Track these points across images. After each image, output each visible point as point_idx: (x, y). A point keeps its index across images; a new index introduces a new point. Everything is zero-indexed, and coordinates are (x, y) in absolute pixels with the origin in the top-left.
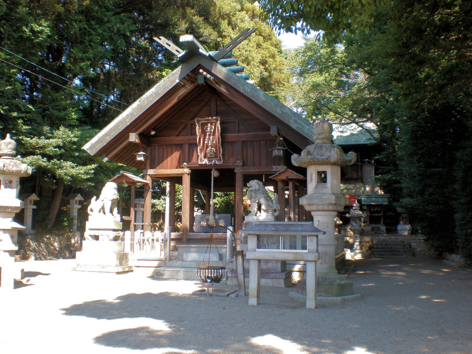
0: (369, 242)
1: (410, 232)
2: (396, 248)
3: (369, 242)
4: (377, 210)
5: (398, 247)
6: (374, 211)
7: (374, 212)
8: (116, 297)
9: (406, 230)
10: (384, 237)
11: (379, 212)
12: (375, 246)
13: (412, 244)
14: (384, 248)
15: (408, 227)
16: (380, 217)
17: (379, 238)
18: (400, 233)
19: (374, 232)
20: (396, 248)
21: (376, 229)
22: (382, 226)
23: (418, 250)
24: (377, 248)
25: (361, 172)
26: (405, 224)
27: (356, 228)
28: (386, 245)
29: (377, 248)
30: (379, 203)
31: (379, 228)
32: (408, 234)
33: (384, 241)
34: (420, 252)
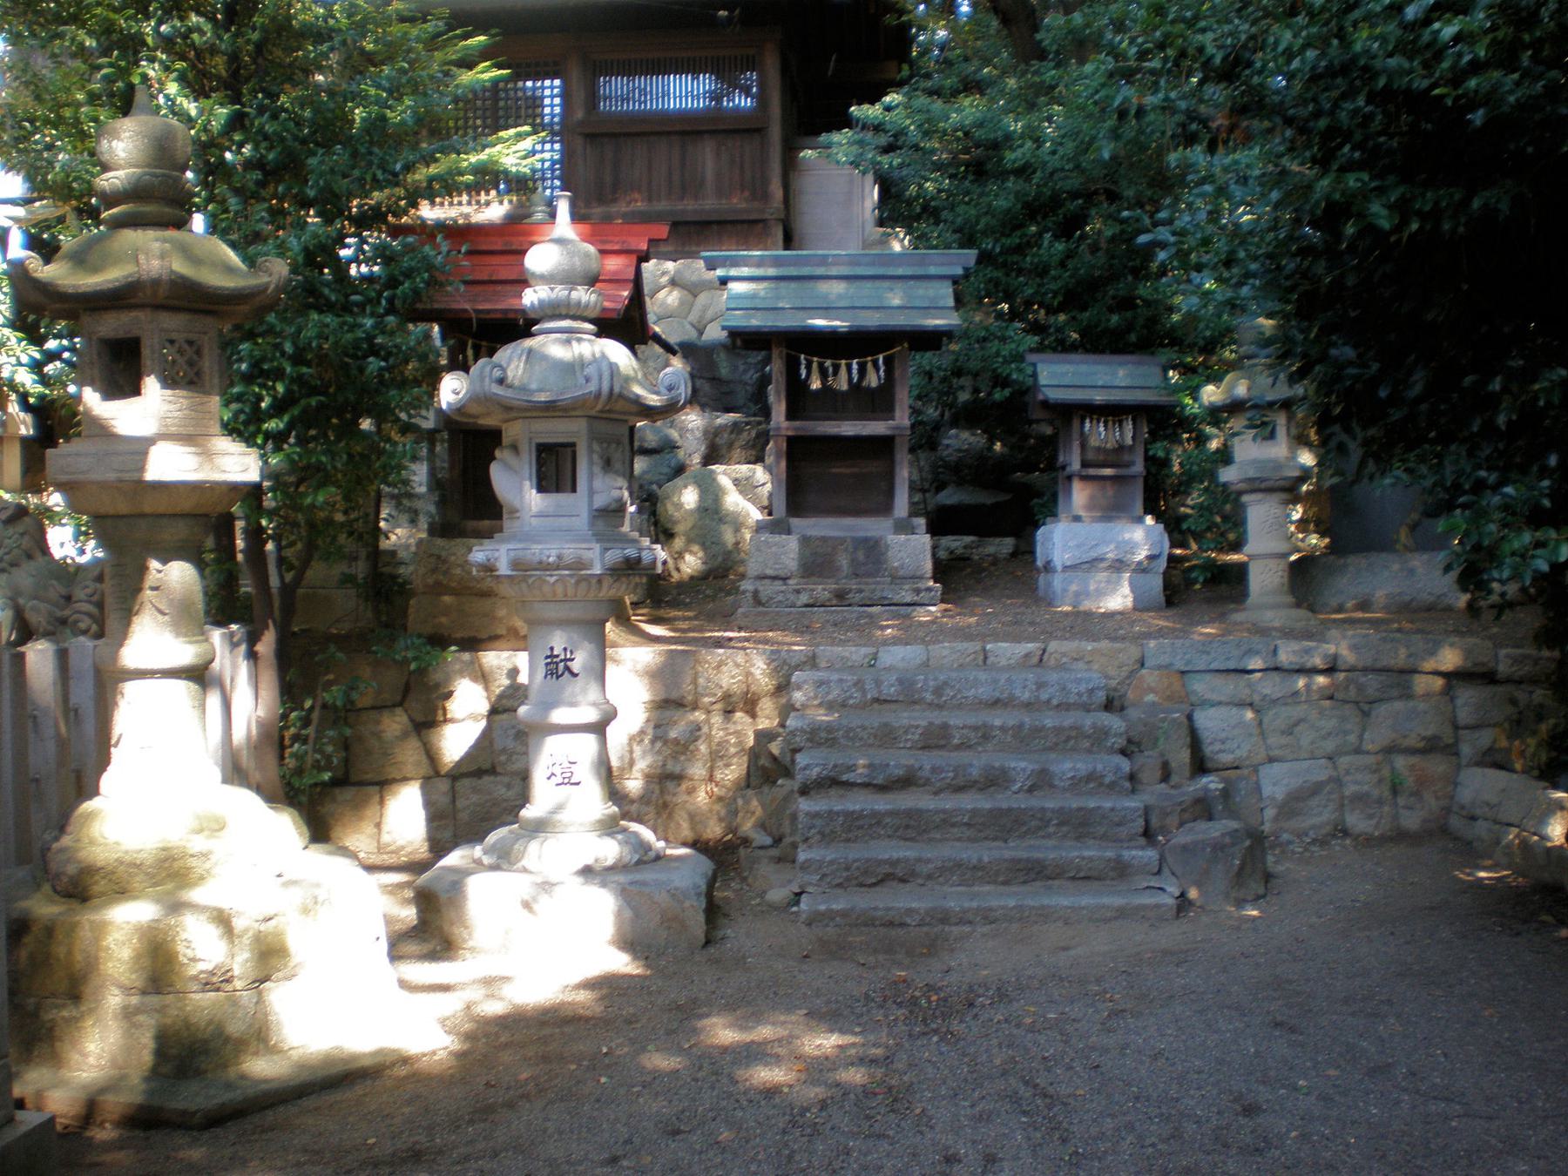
0: (750, 704)
1: (1156, 582)
2: (1041, 781)
3: (750, 704)
4: (856, 388)
5: (1067, 766)
6: (826, 389)
7: (831, 404)
8: (193, 715)
9: (1118, 566)
10: (925, 644)
11: (878, 402)
12: (810, 763)
13: (1209, 722)
14: (906, 782)
15: (1142, 537)
16: (882, 447)
17: (857, 653)
18: (1065, 592)
19: (822, 590)
20: (1041, 781)
21: (843, 561)
22: (903, 527)
23: (1276, 782)
24: (832, 782)
25: (786, 187)
26: (1112, 511)
27: (549, 551)
28: (936, 739)
29: (832, 782)
30: (872, 320)
31: (872, 551)
32: (1140, 606)
33: (909, 696)
34: (1293, 804)
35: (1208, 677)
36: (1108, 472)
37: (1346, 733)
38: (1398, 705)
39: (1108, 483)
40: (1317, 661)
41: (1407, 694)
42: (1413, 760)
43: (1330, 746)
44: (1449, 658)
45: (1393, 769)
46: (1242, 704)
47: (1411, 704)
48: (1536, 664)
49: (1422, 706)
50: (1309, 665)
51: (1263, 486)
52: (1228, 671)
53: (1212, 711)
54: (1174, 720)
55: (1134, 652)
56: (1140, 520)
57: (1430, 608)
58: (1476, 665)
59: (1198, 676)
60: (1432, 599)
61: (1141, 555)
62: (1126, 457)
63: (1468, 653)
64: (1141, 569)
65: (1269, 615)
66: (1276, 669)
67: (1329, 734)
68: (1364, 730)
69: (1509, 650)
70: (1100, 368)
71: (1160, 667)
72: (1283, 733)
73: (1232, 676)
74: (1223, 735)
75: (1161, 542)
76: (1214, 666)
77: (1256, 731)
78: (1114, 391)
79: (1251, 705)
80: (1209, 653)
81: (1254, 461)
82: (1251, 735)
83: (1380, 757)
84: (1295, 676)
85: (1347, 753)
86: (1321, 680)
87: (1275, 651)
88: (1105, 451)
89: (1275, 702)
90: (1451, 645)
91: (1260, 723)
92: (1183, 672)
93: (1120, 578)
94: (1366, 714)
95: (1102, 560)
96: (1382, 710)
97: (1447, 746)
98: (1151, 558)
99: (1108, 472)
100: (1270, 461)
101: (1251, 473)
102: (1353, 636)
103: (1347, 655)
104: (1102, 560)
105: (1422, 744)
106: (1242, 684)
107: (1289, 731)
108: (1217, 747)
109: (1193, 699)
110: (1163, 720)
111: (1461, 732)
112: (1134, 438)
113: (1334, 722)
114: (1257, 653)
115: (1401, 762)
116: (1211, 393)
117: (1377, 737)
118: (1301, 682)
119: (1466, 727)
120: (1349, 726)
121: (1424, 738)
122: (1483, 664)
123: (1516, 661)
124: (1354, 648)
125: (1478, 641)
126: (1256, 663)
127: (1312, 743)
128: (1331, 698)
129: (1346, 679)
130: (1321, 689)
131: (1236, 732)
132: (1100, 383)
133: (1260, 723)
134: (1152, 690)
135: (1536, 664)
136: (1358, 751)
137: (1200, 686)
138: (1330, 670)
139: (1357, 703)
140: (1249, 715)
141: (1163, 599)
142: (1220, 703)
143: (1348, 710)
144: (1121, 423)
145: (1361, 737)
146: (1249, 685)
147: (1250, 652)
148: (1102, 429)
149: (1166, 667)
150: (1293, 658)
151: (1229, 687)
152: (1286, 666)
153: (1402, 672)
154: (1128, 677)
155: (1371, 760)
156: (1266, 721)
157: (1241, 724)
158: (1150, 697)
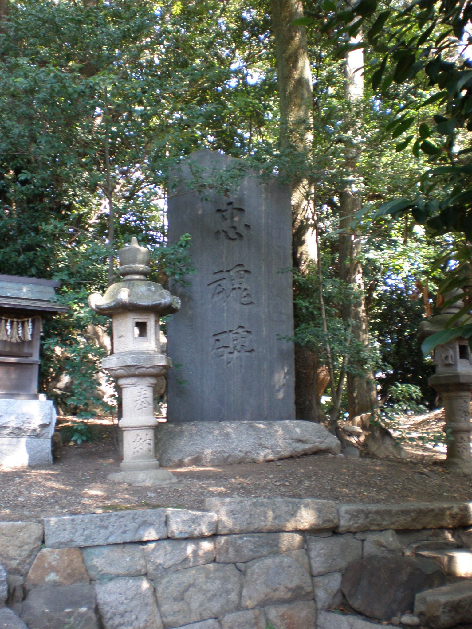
1: (47, 445)
9: (18, 432)
35: (106, 551)
36: (12, 360)
37: (228, 592)
38: (268, 562)
39: (12, 368)
40: (205, 529)
41: (275, 551)
42: (283, 609)
43: (216, 606)
44: (307, 518)
45: (267, 620)
46: (137, 575)
47: (277, 560)
48: (367, 517)
49: (286, 561)
50: (196, 533)
51: (137, 372)
52: (125, 543)
53: (111, 585)
54: (82, 615)
55: (35, 529)
56: (36, 397)
57: (240, 462)
58: (325, 521)
59: (97, 551)
60: (242, 455)
61: (35, 424)
62: (26, 350)
63: (319, 511)
64: (35, 435)
65: (141, 476)
66: (168, 538)
67: (214, 595)
68: (242, 587)
69: (352, 507)
70: (10, 285)
71: (60, 545)
72: (175, 599)
73: (128, 548)
74: (122, 608)
75: (51, 414)
76: (112, 540)
77: (151, 600)
78: (19, 300)
79: (146, 575)
80: (106, 528)
81: (131, 352)
82: (147, 604)
83: (257, 612)
84: (183, 544)
85: (230, 611)
86: (206, 546)
87: (166, 523)
88: (11, 343)
89: (166, 570)
90: (306, 506)
91: (155, 590)
92: (82, 548)
93: (18, 442)
94: (243, 573)
95: (5, 427)
96: (256, 567)
97: (308, 593)
98: (44, 426)
99: (12, 360)
100: (142, 353)
101: (129, 362)
102: (230, 503)
103: (228, 522)
104: (5, 427)
105: (288, 595)
106: (138, 555)
107: (181, 598)
108: (117, 620)
109: (93, 573)
110: (70, 615)
111: (317, 579)
112: (32, 335)
113: (217, 583)
114: (151, 524)
115: (273, 613)
116: (97, 299)
117: (253, 594)
118: (190, 549)
119: (319, 575)
120: (230, 586)
121: (290, 590)
122: (329, 521)
123: (354, 515)
124: (232, 513)
125: (324, 501)
126: (151, 534)
127: (201, 605)
128: (214, 561)
129: (227, 542)
130: (207, 553)
131: (134, 603)
132: (9, 295)
133: (155, 590)
134: (53, 569)
135: (367, 517)
136: (239, 608)
137: (99, 561)
138: (214, 536)
139: (235, 563)
140: (145, 585)
141: (51, 457)
142: (118, 576)
143: (230, 569)
144: (23, 323)
145: (240, 595)
146: (145, 556)
147: (145, 524)
148: (8, 327)
149: (66, 544)
150: (181, 528)
151: (126, 559)
152: (177, 536)
153: (270, 532)
154: (29, 556)
155: (250, 615)
156: (160, 589)
157: (138, 594)
158: (52, 577)
